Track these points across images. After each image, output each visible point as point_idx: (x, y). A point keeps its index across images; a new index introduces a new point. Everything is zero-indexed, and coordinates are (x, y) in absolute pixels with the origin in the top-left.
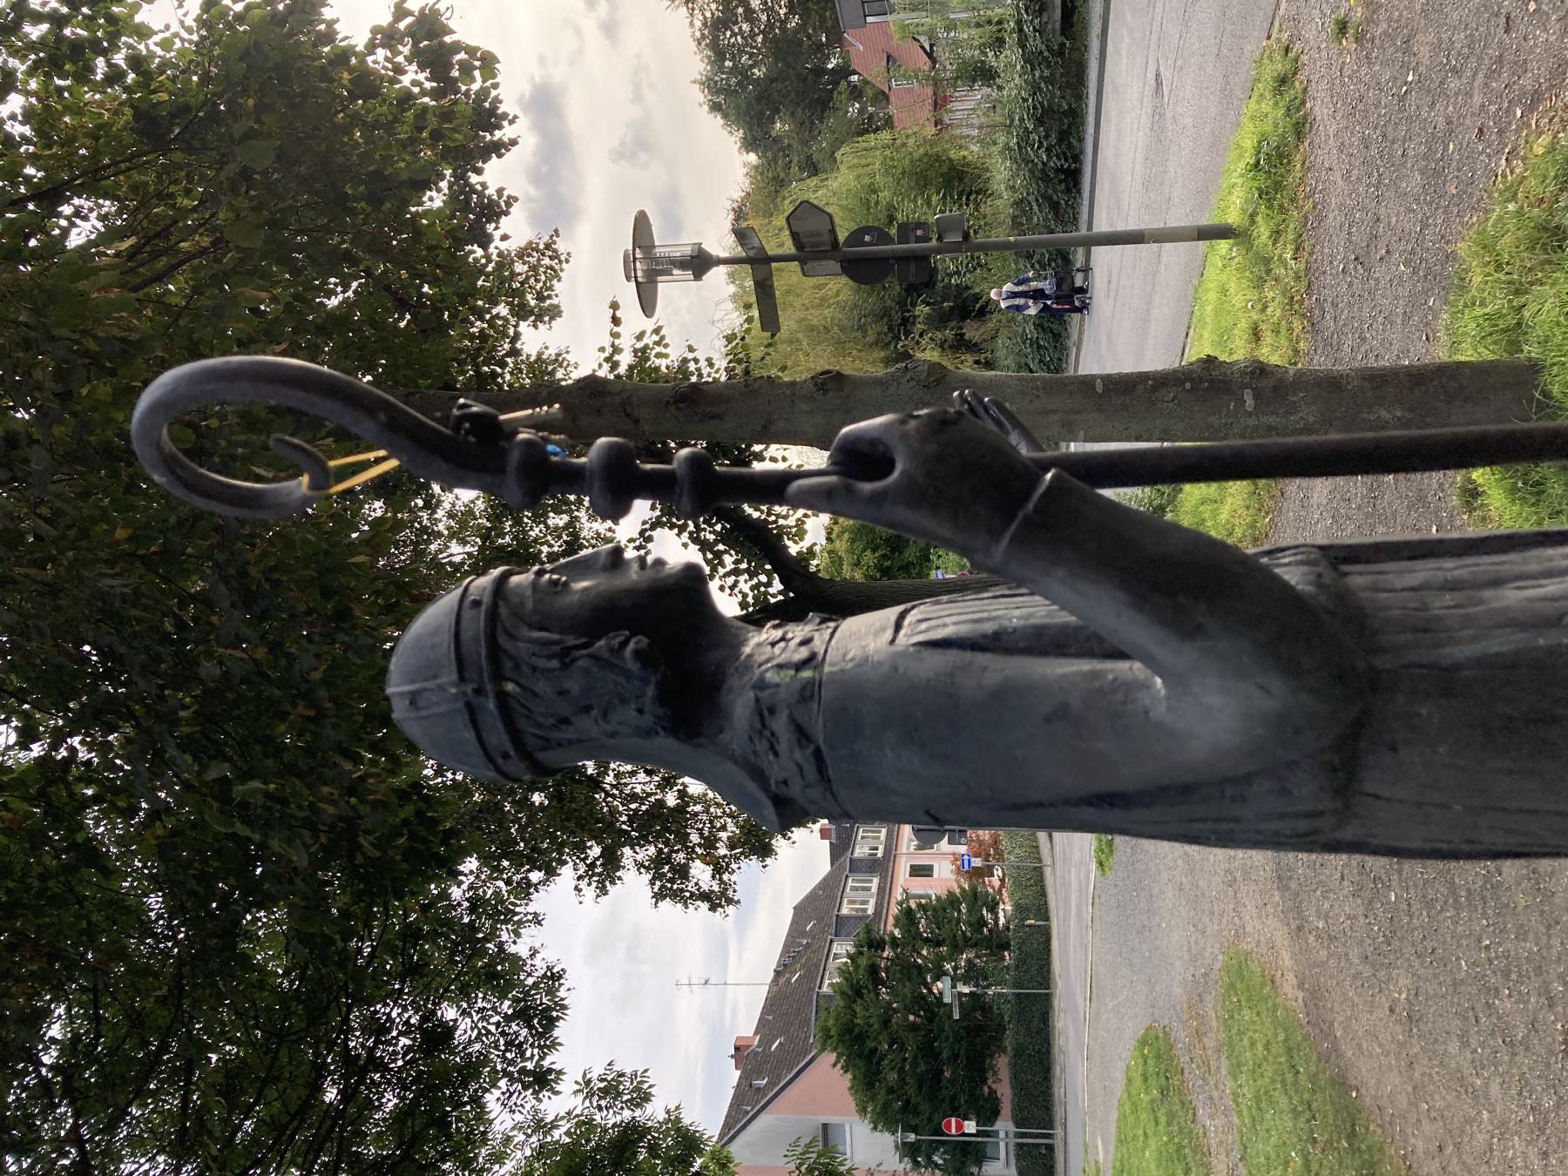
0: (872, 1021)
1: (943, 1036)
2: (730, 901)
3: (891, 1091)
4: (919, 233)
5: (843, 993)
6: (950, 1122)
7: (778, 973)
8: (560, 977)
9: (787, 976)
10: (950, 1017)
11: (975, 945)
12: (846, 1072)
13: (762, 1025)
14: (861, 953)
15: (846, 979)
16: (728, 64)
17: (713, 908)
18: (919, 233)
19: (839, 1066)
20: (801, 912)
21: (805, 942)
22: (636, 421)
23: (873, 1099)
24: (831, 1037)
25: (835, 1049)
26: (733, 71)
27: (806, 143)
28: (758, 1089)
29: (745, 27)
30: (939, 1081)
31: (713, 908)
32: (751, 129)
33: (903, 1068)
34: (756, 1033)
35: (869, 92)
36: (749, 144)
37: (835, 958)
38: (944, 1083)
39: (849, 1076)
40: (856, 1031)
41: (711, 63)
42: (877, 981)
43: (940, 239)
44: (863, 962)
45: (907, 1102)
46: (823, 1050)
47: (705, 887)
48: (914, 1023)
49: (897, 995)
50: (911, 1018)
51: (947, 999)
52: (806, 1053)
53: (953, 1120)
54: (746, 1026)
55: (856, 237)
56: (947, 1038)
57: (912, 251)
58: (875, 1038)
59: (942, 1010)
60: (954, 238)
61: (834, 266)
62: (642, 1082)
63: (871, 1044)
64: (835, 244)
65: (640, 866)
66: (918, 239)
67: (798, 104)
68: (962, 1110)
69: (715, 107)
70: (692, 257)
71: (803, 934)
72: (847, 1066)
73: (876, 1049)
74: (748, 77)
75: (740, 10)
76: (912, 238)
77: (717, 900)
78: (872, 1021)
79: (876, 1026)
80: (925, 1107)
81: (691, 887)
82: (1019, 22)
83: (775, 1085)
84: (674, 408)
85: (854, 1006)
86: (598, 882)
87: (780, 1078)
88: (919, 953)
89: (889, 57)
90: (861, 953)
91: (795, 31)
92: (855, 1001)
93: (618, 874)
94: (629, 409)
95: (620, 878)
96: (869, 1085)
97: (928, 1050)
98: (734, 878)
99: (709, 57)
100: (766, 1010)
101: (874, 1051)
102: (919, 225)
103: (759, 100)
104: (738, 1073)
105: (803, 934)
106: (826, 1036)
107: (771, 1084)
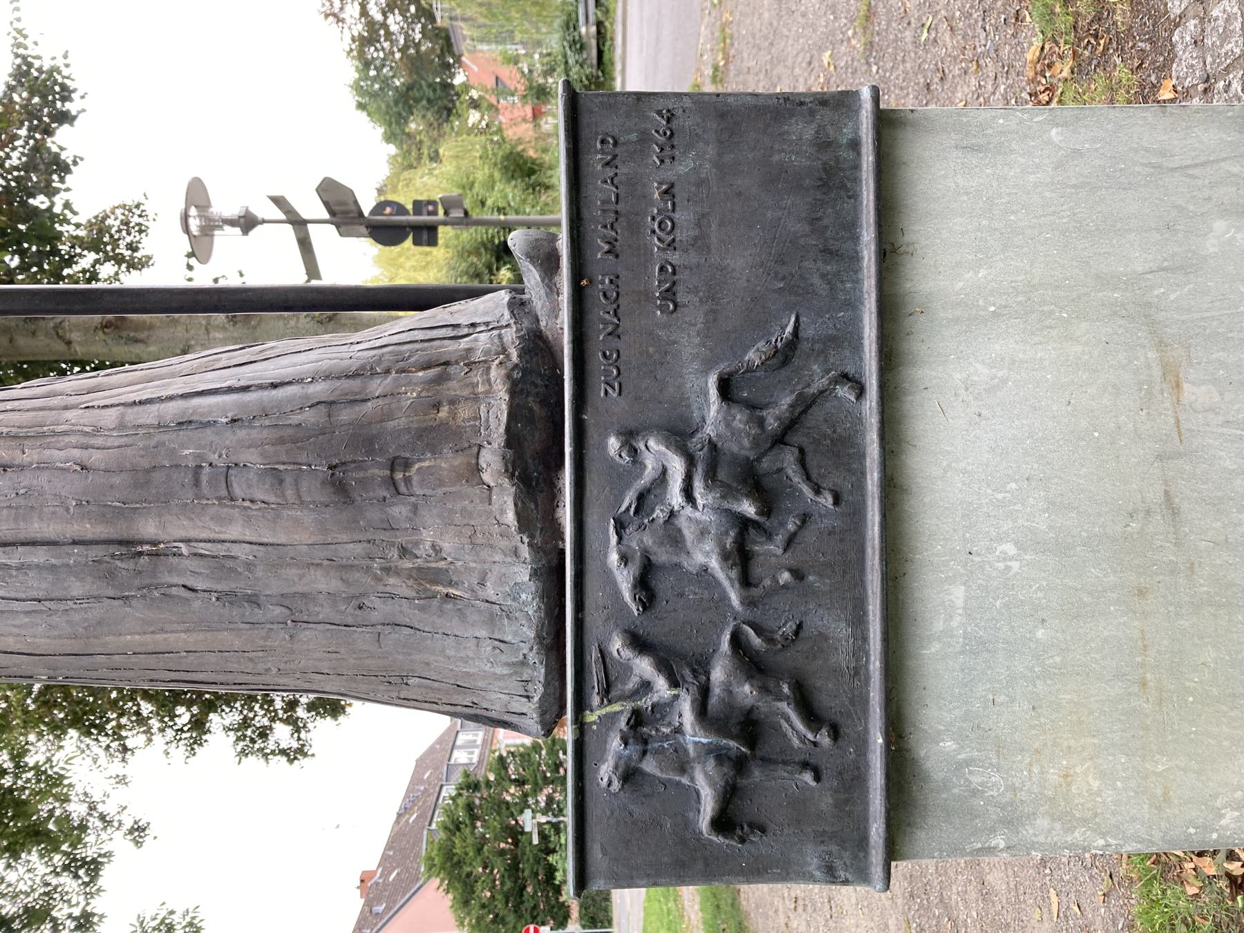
0: (467, 849)
1: (525, 858)
2: (305, 755)
3: (483, 906)
4: (430, 208)
5: (446, 828)
6: (528, 929)
7: (399, 815)
8: (144, 830)
9: (407, 816)
10: (531, 843)
11: (552, 782)
12: (448, 892)
13: (385, 859)
14: (460, 795)
15: (448, 816)
16: (372, 73)
17: (291, 761)
18: (430, 208)
19: (442, 889)
20: (421, 764)
21: (422, 788)
22: (69, 343)
23: (469, 914)
24: (435, 865)
25: (438, 875)
26: (374, 79)
27: (435, 141)
28: (377, 914)
29: (386, 45)
30: (522, 895)
31: (291, 761)
32: (390, 125)
33: (494, 887)
34: (379, 866)
35: (485, 105)
36: (390, 137)
37: (444, 800)
38: (525, 897)
39: (450, 896)
40: (455, 859)
41: (357, 70)
42: (474, 818)
43: (446, 213)
44: (461, 801)
45: (497, 916)
46: (429, 877)
47: (284, 745)
48: (503, 850)
49: (488, 828)
50: (502, 845)
51: (527, 829)
52: (418, 879)
53: (532, 927)
54: (371, 862)
55: (379, 208)
56: (528, 860)
57: (424, 222)
58: (471, 864)
59: (524, 837)
60: (457, 214)
61: (363, 229)
62: (194, 918)
63: (467, 869)
64: (361, 214)
65: (227, 729)
66: (429, 213)
67: (428, 109)
68: (539, 919)
69: (361, 106)
70: (240, 217)
71: (421, 782)
72: (448, 889)
73: (472, 872)
74: (388, 85)
75: (382, 32)
76: (425, 211)
77: (293, 755)
78: (467, 849)
79: (471, 854)
80: (511, 918)
81: (271, 745)
82: (565, 56)
83: (391, 908)
84: (101, 333)
85: (453, 838)
86: (186, 745)
87: (395, 902)
88: (507, 791)
89: (497, 78)
90: (460, 795)
91: (426, 52)
92: (455, 834)
93: (204, 737)
94: (60, 332)
95: (206, 741)
96: (466, 903)
97: (513, 869)
98: (309, 735)
99: (357, 67)
100: (389, 846)
101: (469, 875)
102: (429, 202)
103: (396, 103)
104: (363, 901)
105: (421, 782)
106: (431, 867)
107: (388, 909)
